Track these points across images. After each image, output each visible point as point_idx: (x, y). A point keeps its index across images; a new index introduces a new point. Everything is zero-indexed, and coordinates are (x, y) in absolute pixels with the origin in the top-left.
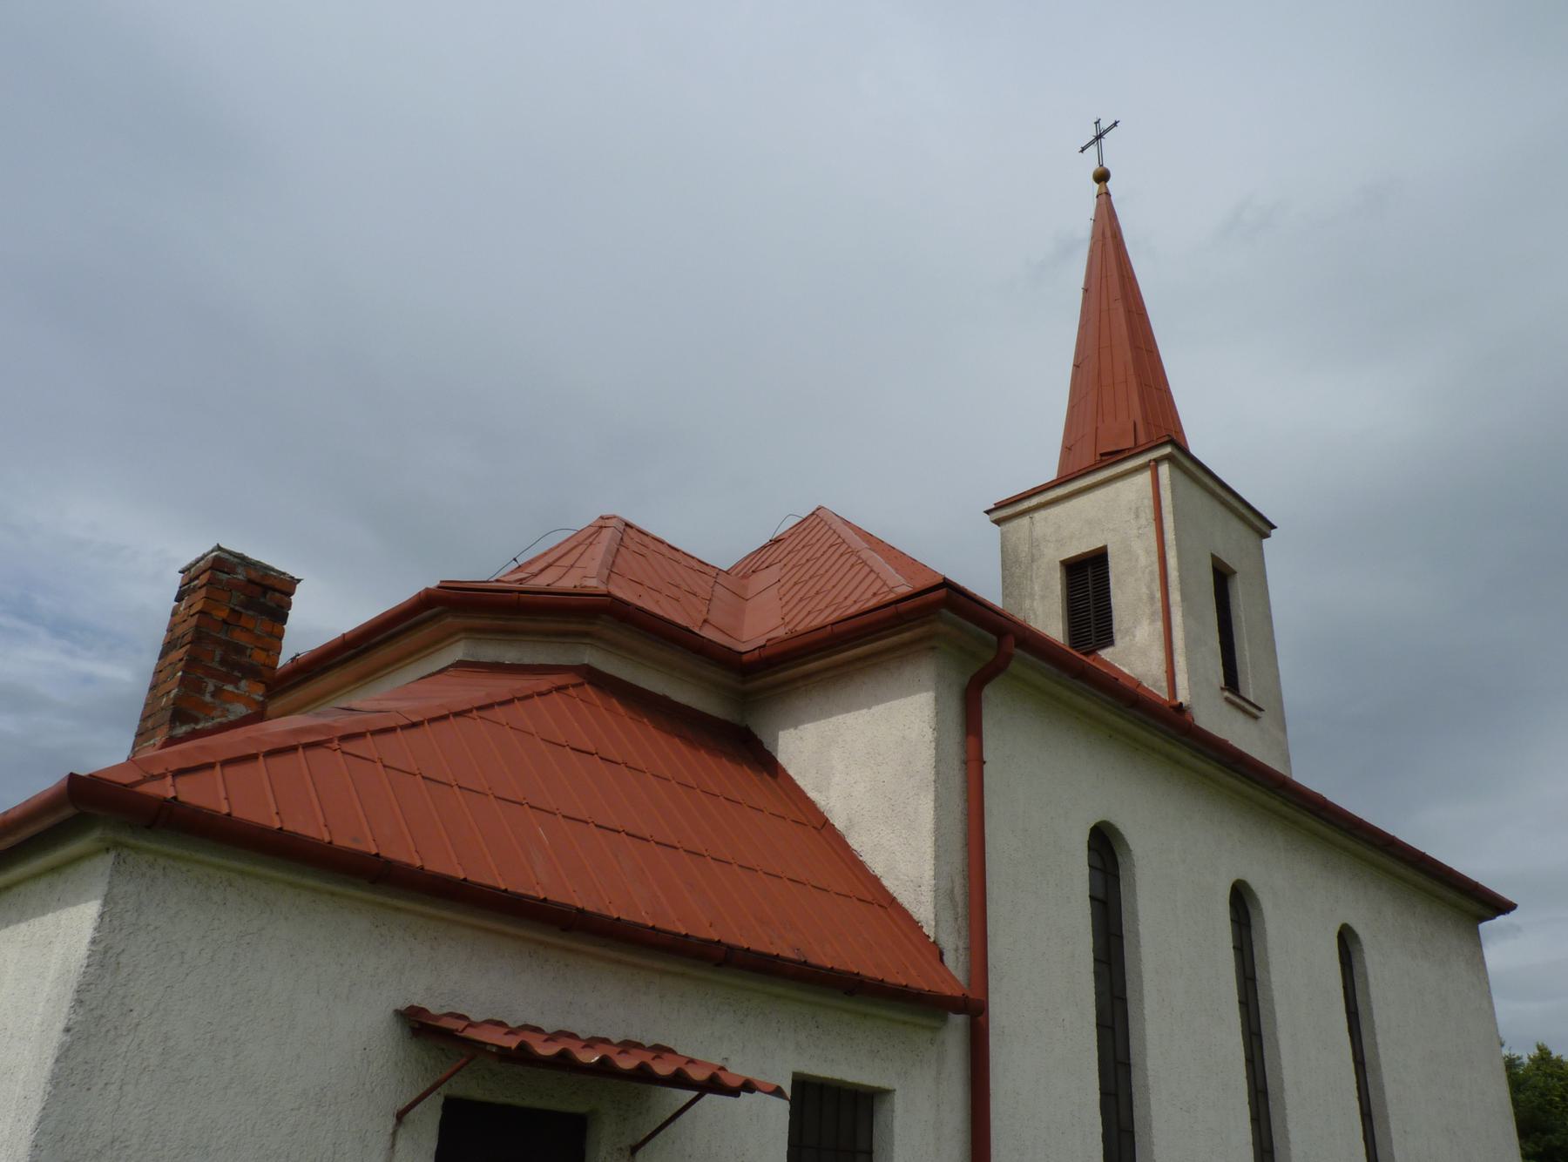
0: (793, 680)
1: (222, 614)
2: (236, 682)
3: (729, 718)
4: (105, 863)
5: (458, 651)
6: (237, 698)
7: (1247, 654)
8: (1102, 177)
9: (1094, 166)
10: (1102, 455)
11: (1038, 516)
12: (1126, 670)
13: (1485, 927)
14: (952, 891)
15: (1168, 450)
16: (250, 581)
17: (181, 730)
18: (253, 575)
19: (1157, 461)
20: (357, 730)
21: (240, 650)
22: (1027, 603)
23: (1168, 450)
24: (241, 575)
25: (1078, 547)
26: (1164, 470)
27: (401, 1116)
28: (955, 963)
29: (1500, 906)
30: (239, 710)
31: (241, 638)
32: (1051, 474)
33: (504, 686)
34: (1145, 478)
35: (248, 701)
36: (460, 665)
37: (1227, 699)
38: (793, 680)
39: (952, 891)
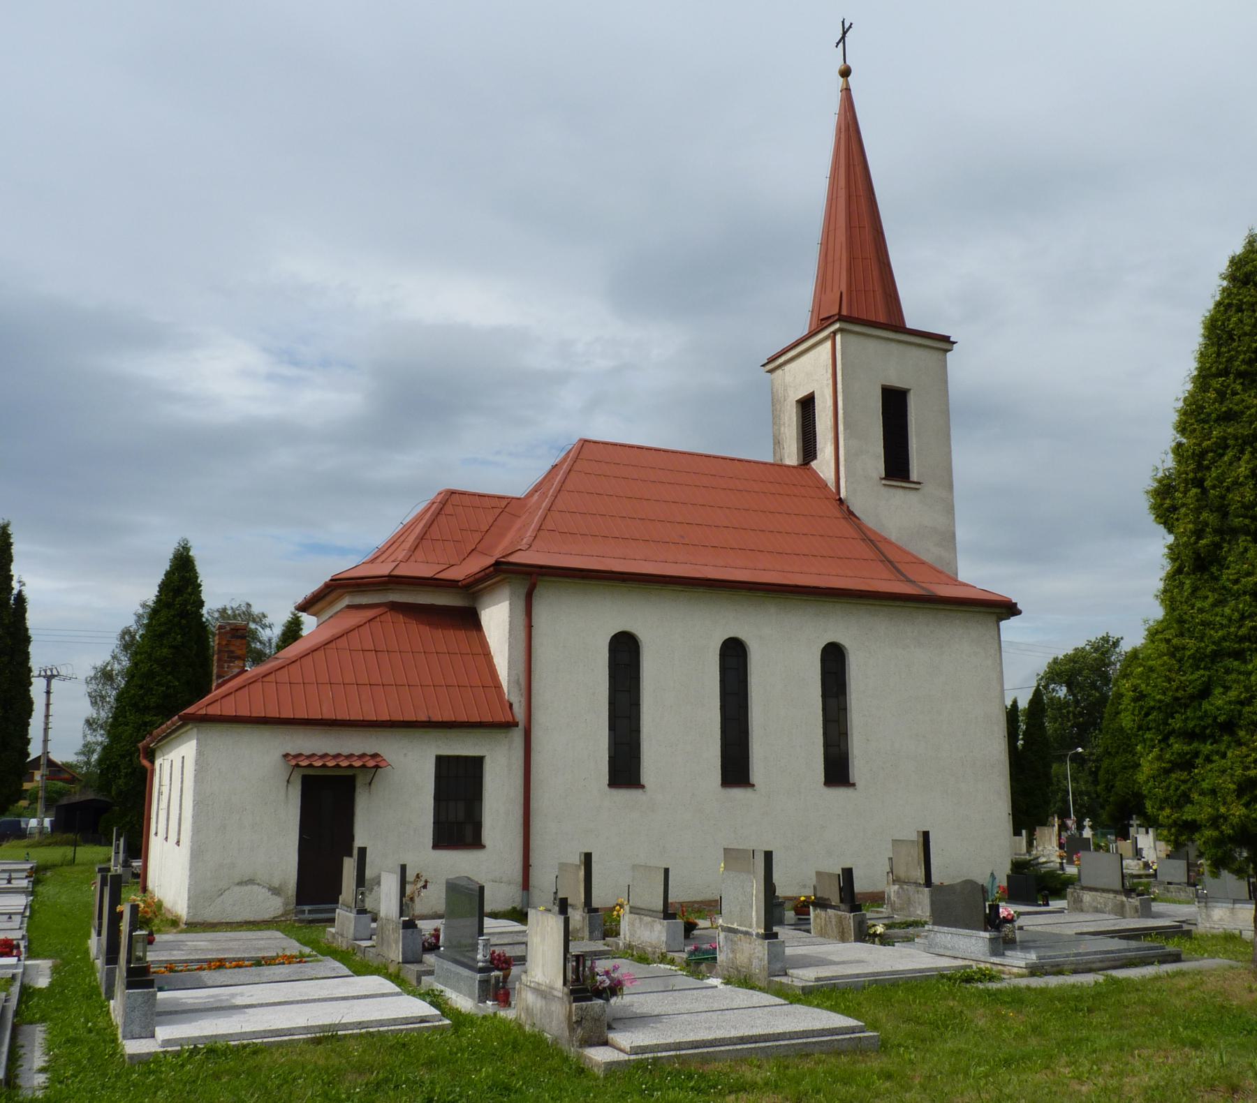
0: (485, 588)
1: (224, 643)
2: (233, 662)
3: (467, 605)
4: (195, 730)
5: (346, 601)
6: (234, 667)
7: (915, 446)
8: (845, 73)
9: (839, 64)
10: (822, 320)
11: (787, 367)
12: (822, 476)
13: (1003, 624)
14: (518, 679)
15: (837, 326)
16: (232, 629)
17: (220, 681)
18: (232, 627)
19: (834, 333)
20: (354, 611)
21: (232, 652)
22: (782, 429)
23: (837, 326)
24: (228, 629)
25: (802, 394)
26: (838, 337)
27: (288, 781)
28: (519, 712)
29: (1008, 609)
30: (236, 671)
31: (232, 648)
32: (805, 331)
33: (370, 614)
34: (828, 344)
35: (238, 667)
36: (349, 607)
37: (885, 485)
38: (485, 588)
39: (518, 679)
